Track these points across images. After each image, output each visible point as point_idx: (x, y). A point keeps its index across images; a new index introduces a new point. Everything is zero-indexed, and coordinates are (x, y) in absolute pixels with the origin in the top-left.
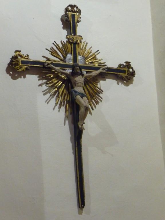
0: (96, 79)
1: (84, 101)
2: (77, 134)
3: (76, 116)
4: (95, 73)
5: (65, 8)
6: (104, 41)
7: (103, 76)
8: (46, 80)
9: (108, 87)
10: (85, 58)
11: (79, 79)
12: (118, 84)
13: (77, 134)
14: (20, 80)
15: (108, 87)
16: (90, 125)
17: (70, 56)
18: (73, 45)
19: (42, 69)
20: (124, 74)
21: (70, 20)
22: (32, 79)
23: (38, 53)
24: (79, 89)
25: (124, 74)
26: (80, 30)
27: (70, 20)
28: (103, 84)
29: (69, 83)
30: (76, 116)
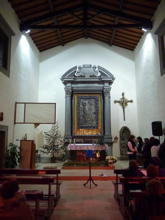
0: (127, 103)
1: (124, 106)
2: (124, 111)
3: (124, 108)
4: (127, 102)
5: (152, 122)
6: (128, 97)
7: (128, 102)
8: (35, 164)
9: (129, 104)
10: (125, 100)
11: (124, 103)
12: (115, 78)
13: (124, 111)
14: (116, 104)
15: (129, 104)
16: (126, 109)
17: (123, 100)
18: (123, 98)
19: (119, 102)
20: (131, 101)
21: (123, 94)
22: (118, 103)
23: (118, 100)
24: (124, 104)
25: (131, 101)
26: (124, 96)
27: (123, 94)
28: (128, 103)
29: (123, 104)
30: (124, 108)
